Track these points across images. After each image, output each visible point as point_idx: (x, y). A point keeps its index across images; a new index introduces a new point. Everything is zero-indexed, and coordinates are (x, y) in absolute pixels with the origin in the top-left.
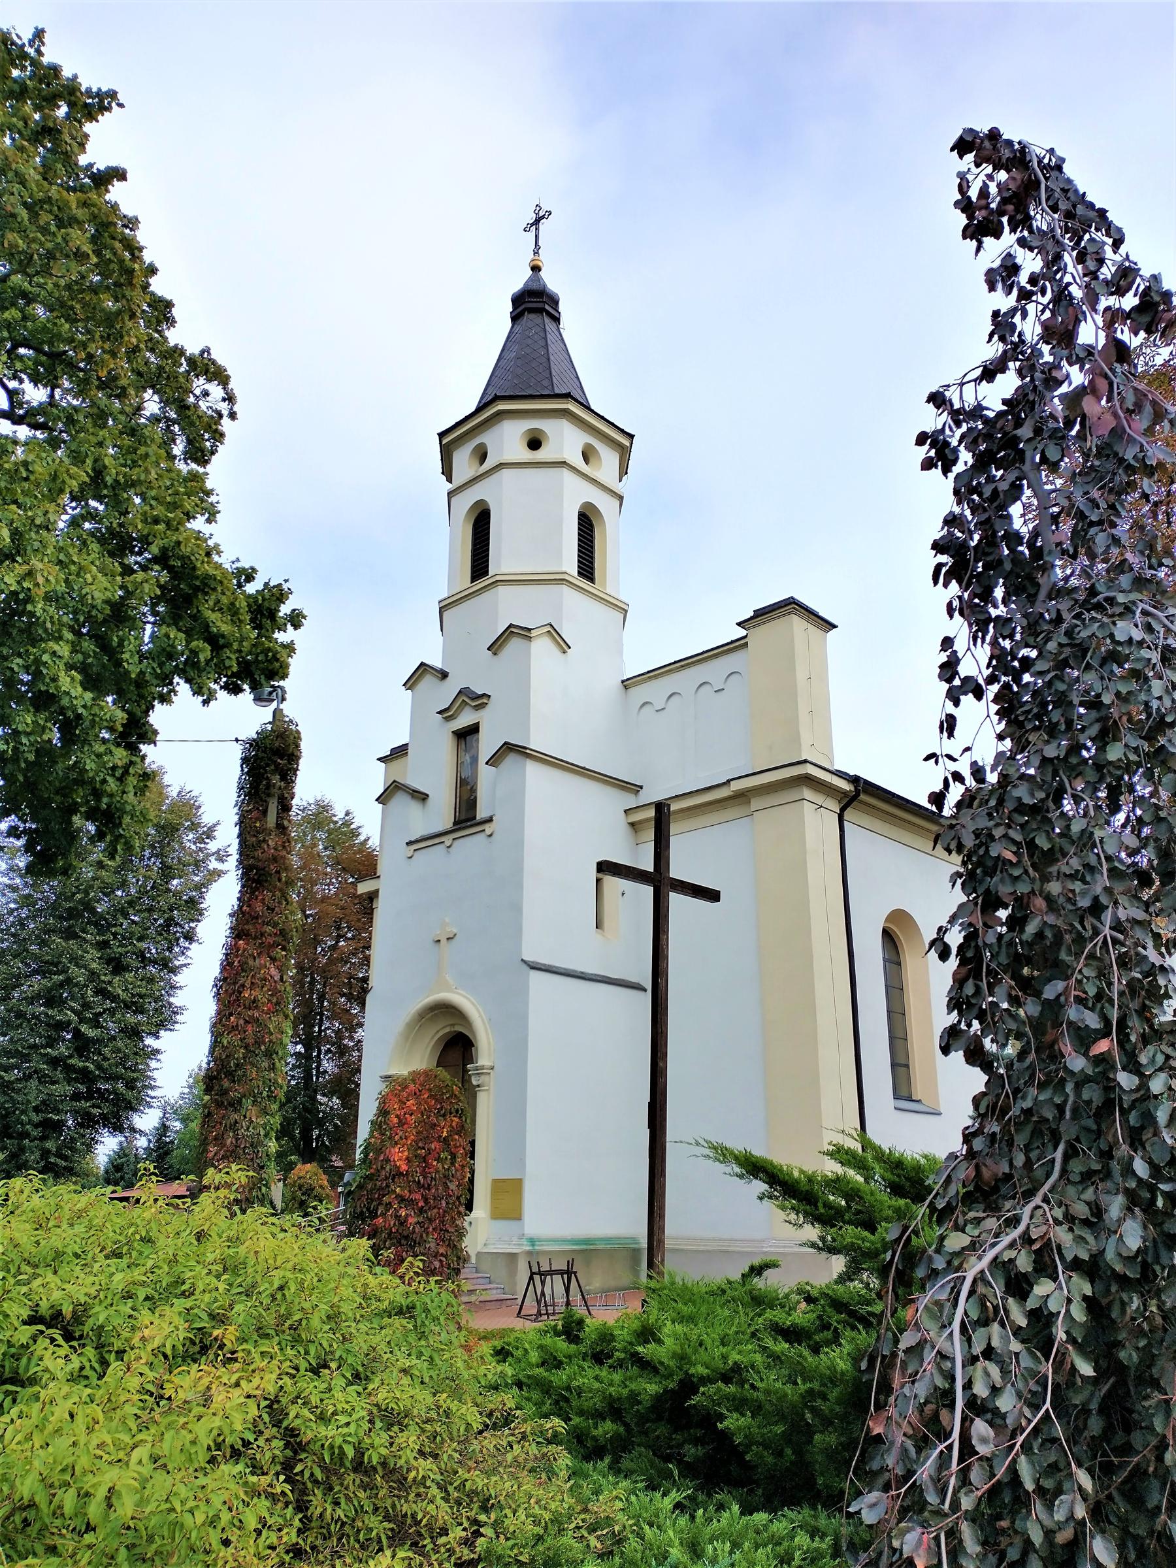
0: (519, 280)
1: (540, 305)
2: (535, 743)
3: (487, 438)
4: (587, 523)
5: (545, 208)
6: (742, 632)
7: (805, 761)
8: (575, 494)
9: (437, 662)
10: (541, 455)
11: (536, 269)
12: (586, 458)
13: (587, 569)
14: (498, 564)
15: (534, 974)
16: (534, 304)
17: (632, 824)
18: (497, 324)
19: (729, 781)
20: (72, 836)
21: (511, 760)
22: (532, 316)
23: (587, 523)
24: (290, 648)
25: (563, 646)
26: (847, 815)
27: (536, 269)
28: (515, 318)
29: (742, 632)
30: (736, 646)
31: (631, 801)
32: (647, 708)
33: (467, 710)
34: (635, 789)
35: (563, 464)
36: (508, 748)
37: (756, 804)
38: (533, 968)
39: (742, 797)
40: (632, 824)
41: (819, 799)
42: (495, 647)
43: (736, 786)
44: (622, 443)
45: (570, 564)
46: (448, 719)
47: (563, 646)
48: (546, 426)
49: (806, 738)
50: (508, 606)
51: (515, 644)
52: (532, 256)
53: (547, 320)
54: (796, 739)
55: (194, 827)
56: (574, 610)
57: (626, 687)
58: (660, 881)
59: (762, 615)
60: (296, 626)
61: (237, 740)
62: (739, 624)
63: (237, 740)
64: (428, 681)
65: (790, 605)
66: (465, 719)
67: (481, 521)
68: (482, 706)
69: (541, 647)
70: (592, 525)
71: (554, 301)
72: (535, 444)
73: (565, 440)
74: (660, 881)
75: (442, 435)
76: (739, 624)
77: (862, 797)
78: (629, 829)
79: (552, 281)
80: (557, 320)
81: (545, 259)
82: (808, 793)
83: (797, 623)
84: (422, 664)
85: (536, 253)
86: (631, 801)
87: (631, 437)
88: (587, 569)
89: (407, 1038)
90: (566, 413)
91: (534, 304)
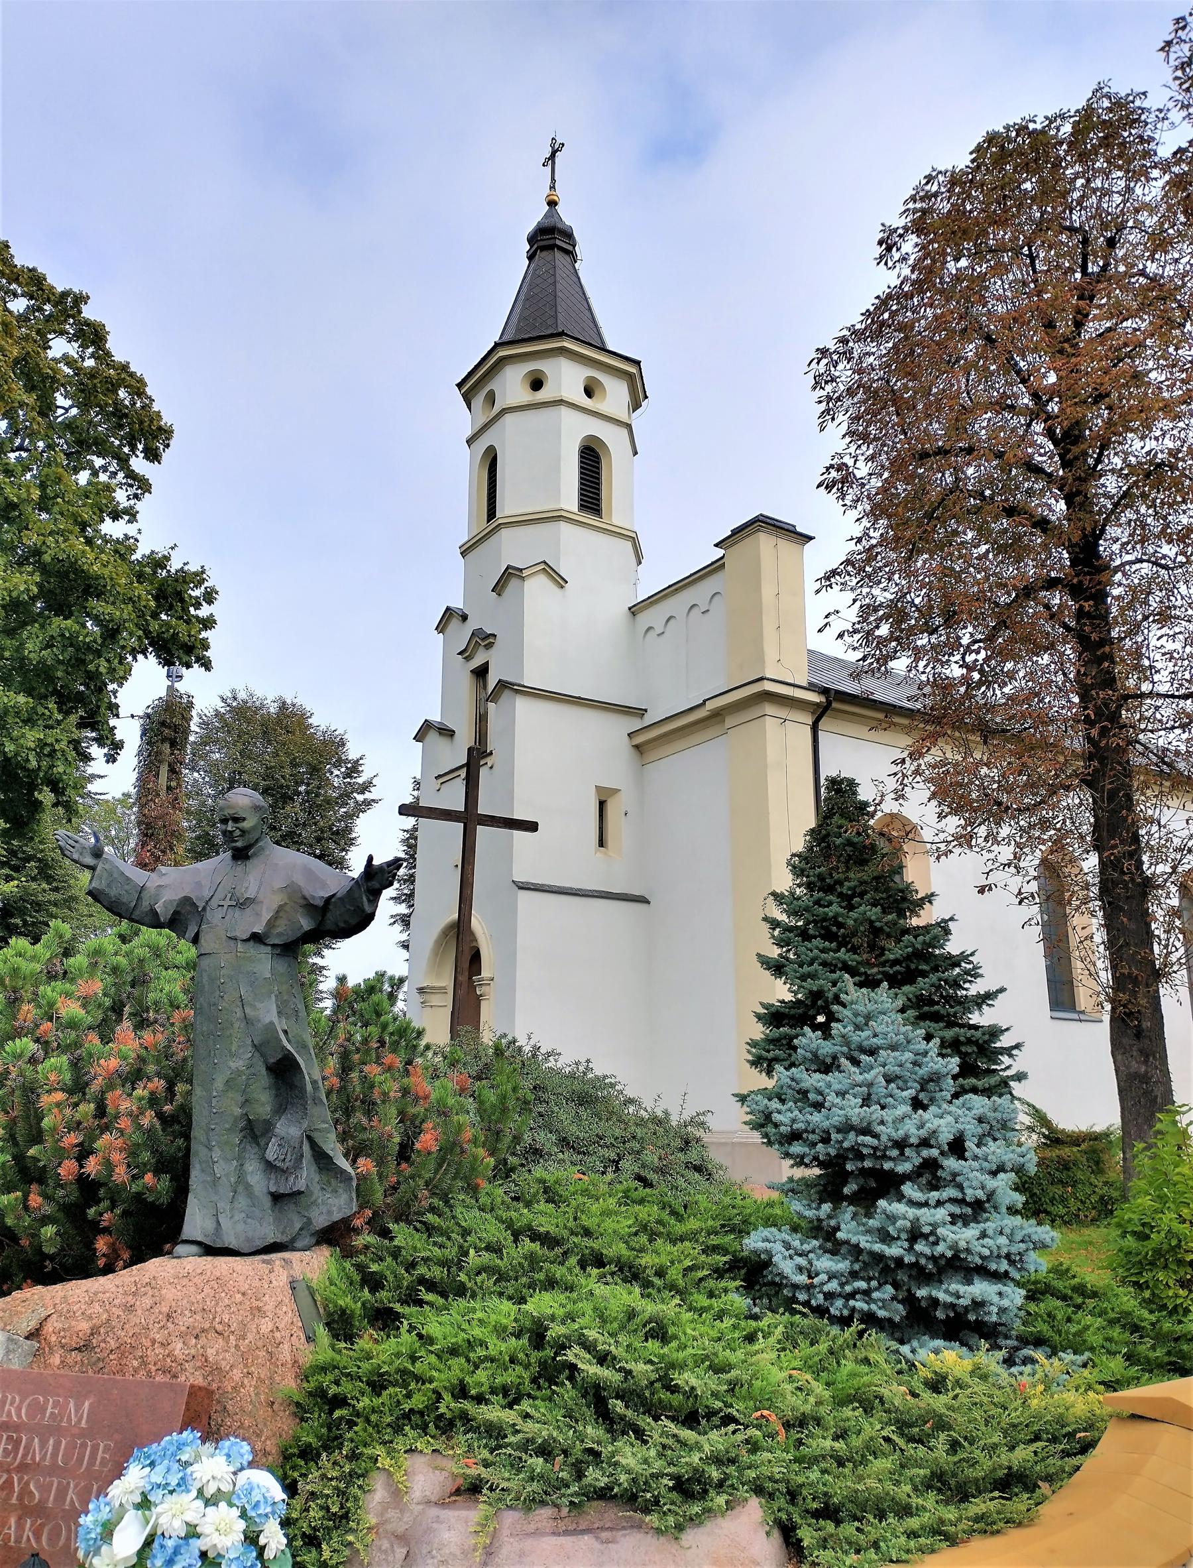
0: (536, 215)
1: (551, 242)
2: (530, 679)
3: (494, 385)
4: (591, 458)
5: (559, 141)
6: (720, 552)
7: (762, 679)
8: (573, 430)
9: (458, 603)
10: (543, 395)
11: (552, 204)
12: (589, 392)
13: (591, 497)
14: (505, 509)
15: (523, 894)
16: (551, 240)
17: (637, 747)
18: (514, 265)
19: (705, 701)
20: (37, 806)
21: (507, 694)
22: (545, 254)
23: (591, 458)
24: (208, 623)
25: (560, 581)
26: (821, 725)
27: (552, 204)
28: (531, 258)
29: (720, 552)
30: (716, 567)
31: (636, 724)
32: (650, 633)
33: (481, 649)
34: (641, 712)
35: (561, 402)
36: (503, 685)
37: (730, 721)
38: (521, 888)
39: (718, 716)
40: (637, 747)
41: (783, 713)
42: (498, 588)
43: (710, 706)
44: (631, 374)
45: (570, 500)
46: (468, 659)
47: (560, 581)
48: (545, 366)
49: (771, 654)
50: (513, 548)
51: (514, 583)
52: (548, 191)
53: (558, 255)
54: (760, 659)
55: (339, 763)
56: (575, 546)
57: (634, 614)
58: (470, 818)
59: (739, 533)
60: (210, 602)
61: (132, 716)
62: (716, 545)
63: (132, 716)
64: (455, 623)
65: (762, 523)
66: (477, 662)
67: (491, 462)
68: (489, 646)
69: (536, 589)
70: (598, 457)
71: (568, 235)
72: (537, 384)
73: (566, 378)
74: (470, 818)
75: (459, 386)
76: (716, 545)
77: (834, 705)
78: (632, 750)
79: (568, 215)
80: (571, 254)
81: (561, 193)
82: (770, 709)
83: (765, 541)
84: (448, 609)
85: (553, 187)
86: (636, 724)
87: (638, 363)
88: (591, 497)
89: (437, 955)
90: (562, 351)
91: (551, 240)
